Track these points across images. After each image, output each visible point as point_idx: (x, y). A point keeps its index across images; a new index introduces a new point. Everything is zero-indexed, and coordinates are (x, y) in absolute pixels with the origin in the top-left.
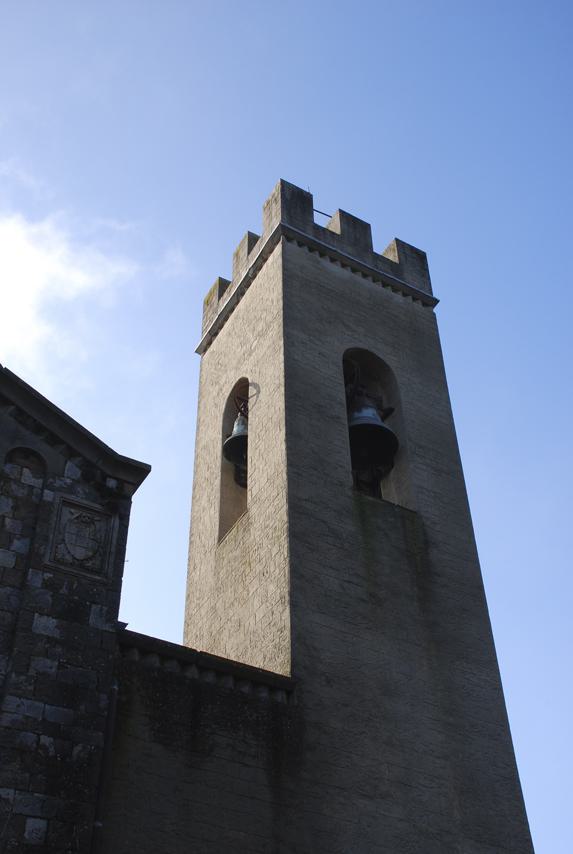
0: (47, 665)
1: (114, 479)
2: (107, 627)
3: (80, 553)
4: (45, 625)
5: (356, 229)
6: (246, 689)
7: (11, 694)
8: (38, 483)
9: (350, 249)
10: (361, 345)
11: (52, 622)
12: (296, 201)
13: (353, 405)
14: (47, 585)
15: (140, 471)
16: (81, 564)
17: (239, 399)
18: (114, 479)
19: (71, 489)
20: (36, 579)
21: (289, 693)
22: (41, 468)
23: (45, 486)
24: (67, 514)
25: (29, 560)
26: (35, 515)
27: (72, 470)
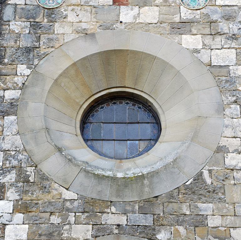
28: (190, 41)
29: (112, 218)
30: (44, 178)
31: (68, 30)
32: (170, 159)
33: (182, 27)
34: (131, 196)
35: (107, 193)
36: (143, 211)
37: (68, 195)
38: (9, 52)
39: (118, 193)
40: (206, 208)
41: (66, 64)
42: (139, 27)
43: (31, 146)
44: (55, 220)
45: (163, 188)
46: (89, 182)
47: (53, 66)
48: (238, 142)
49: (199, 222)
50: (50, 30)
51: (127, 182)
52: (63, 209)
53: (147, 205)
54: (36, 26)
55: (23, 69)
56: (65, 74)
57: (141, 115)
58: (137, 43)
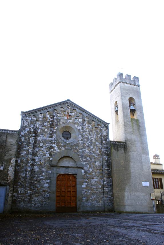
0: (105, 145)
1: (106, 125)
2: (109, 141)
3: (105, 134)
4: (104, 142)
5: (129, 76)
6: (121, 144)
7: (163, 233)
8: (100, 127)
9: (128, 81)
10: (129, 97)
11: (104, 141)
12: (121, 75)
13: (130, 106)
14: (103, 138)
15: (109, 124)
16: (106, 135)
17: (116, 103)
18: (106, 125)
19: (103, 127)
20: (102, 137)
21: (125, 143)
22: (100, 126)
23: (101, 128)
24: (104, 130)
25: (101, 136)
26: (101, 131)
27: (103, 125)
28: (76, 125)
29: (67, 148)
30: (59, 142)
31: (61, 122)
32: (73, 141)
33: (75, 123)
34: (69, 145)
35: (66, 145)
36: (70, 147)
37: (62, 144)
38: (55, 125)
39: (67, 145)
40: (77, 147)
41: (61, 127)
42: (83, 116)
43: (58, 138)
44: (60, 147)
45: (72, 145)
46: (64, 143)
47: (60, 127)
48: (163, 229)
49: (76, 149)
50: (59, 122)
51: (68, 143)
52: (61, 146)
53: (71, 146)
54: (58, 121)
55: (56, 127)
56: (61, 128)
57: (69, 134)
58: (70, 125)
